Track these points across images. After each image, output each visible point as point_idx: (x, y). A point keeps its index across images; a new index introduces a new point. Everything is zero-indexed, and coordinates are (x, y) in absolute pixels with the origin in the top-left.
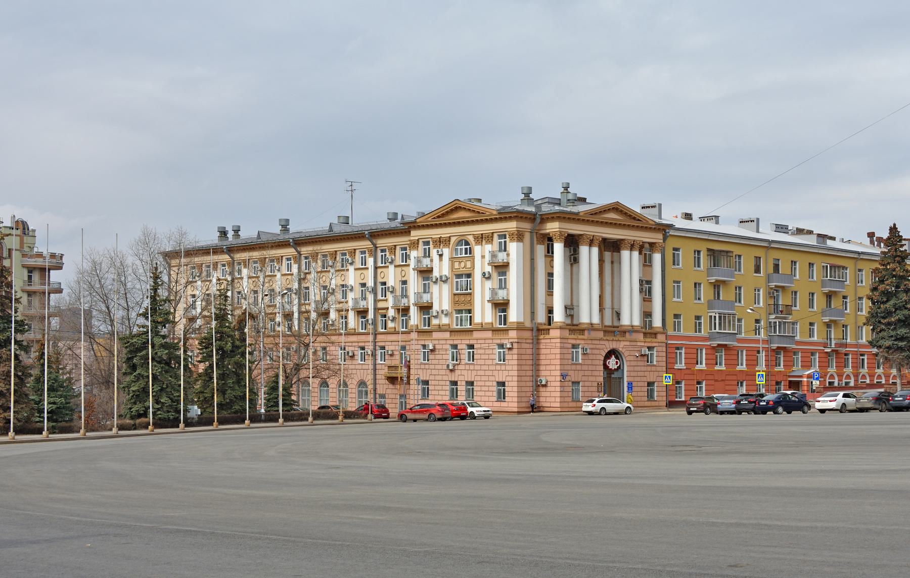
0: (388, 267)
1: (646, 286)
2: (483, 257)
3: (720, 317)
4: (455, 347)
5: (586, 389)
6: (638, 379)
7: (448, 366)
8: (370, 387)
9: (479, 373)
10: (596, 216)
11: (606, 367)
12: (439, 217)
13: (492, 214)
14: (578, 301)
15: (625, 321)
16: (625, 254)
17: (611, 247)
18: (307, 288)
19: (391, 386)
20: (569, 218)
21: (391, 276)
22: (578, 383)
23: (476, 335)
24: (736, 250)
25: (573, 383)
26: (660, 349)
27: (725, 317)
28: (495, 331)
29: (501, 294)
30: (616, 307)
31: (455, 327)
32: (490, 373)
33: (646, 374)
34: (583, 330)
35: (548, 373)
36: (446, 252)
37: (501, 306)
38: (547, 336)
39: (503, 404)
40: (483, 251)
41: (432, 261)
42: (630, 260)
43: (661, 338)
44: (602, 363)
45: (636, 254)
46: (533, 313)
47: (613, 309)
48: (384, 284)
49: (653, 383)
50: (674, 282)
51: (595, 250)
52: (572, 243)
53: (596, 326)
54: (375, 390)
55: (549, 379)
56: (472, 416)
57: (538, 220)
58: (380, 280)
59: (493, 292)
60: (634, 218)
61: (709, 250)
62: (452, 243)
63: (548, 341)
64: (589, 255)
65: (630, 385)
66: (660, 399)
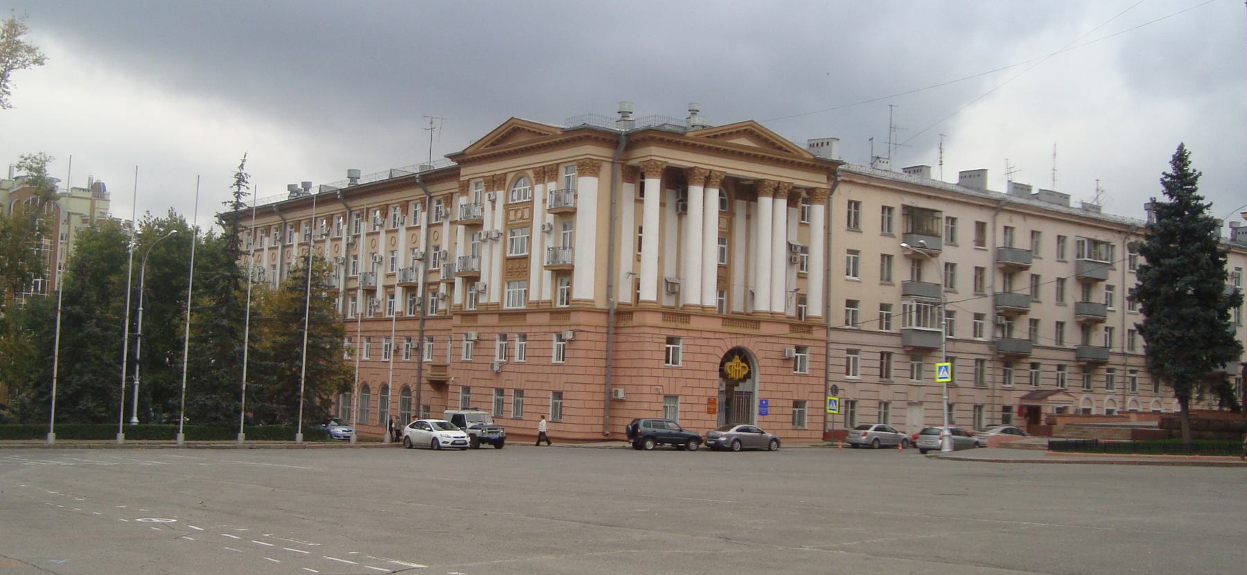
0: (441, 224)
1: (797, 255)
2: (544, 201)
3: (918, 308)
4: (504, 337)
5: (688, 408)
6: (779, 395)
7: (492, 366)
8: (414, 394)
10: (714, 142)
11: (722, 373)
12: (493, 144)
13: (555, 136)
15: (762, 305)
16: (765, 202)
18: (356, 257)
19: (437, 394)
20: (669, 141)
21: (454, 242)
22: (676, 397)
23: (530, 319)
24: (948, 210)
25: (666, 397)
26: (815, 350)
27: (926, 308)
28: (555, 313)
29: (565, 257)
30: (751, 284)
32: (543, 378)
36: (500, 195)
37: (563, 273)
39: (560, 427)
41: (483, 210)
42: (772, 210)
43: (819, 334)
44: (717, 367)
45: (782, 203)
46: (610, 287)
48: (437, 248)
49: (676, 397)
50: (849, 251)
51: (714, 194)
52: (677, 181)
53: (709, 312)
54: (419, 398)
56: (409, 444)
57: (623, 144)
58: (433, 243)
59: (555, 253)
60: (780, 148)
61: (905, 207)
62: (508, 182)
64: (704, 203)
65: (764, 405)
66: (814, 426)
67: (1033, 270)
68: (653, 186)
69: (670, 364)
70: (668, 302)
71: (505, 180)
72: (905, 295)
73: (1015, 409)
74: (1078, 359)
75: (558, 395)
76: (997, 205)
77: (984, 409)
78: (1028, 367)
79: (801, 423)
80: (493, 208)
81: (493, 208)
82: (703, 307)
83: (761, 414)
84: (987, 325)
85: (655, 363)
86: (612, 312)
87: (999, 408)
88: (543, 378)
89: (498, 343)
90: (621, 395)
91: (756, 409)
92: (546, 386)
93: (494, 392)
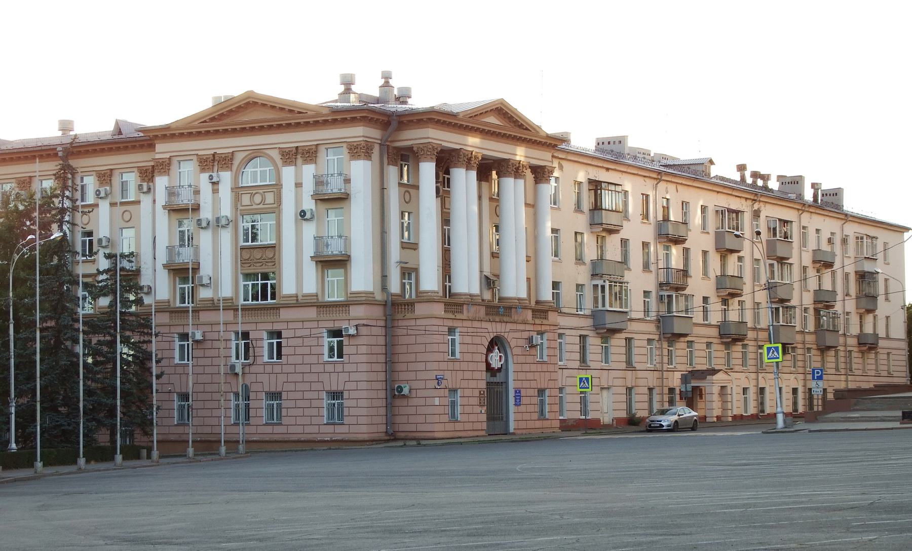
2: (298, 185)
9: (292, 378)
14: (169, 282)
17: (487, 169)
23: (285, 314)
31: (178, 304)
32: (314, 377)
33: (537, 375)
34: (461, 305)
35: (412, 376)
36: (226, 177)
38: (409, 315)
39: (339, 429)
40: (298, 175)
46: (384, 277)
47: (481, 272)
48: (90, 234)
55: (415, 385)
56: (659, 429)
57: (394, 124)
63: (413, 323)
64: (464, 180)
67: (623, 234)
68: (428, 170)
69: (335, 359)
70: (487, 296)
71: (232, 159)
72: (594, 276)
73: (677, 392)
74: (721, 336)
75: (336, 395)
76: (724, 186)
77: (655, 392)
78: (684, 345)
79: (341, 416)
80: (215, 191)
81: (215, 191)
82: (471, 295)
83: (516, 405)
84: (653, 300)
85: (440, 357)
86: (389, 304)
87: (666, 390)
88: (530, 376)
89: (326, 340)
90: (406, 391)
91: (512, 401)
92: (319, 386)
93: (324, 395)
